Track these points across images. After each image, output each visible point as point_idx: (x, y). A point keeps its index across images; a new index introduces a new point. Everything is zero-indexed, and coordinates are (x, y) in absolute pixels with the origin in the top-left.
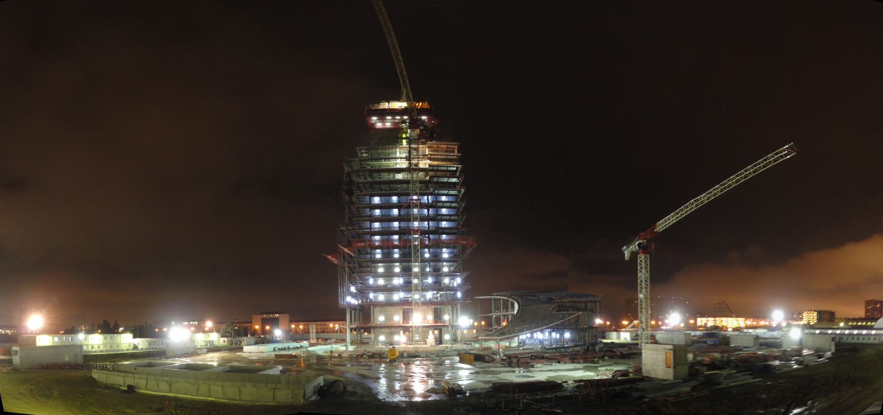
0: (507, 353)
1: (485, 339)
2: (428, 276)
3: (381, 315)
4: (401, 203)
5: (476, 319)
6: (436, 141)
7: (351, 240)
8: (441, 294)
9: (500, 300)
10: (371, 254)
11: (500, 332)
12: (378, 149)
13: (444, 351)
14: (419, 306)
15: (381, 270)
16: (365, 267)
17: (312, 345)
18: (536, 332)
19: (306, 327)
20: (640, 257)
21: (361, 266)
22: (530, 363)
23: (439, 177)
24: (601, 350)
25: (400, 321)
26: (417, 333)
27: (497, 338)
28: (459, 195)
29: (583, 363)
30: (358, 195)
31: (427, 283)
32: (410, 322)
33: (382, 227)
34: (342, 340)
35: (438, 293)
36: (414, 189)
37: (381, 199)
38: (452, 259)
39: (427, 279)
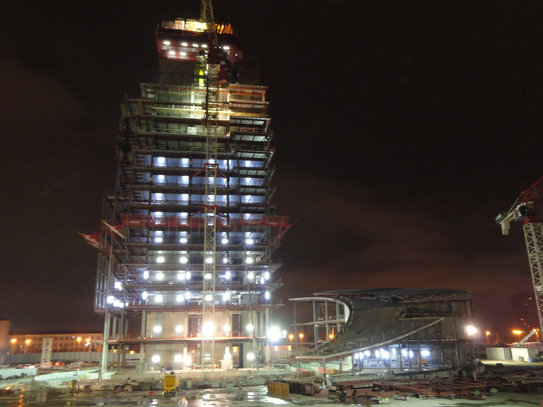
0: (337, 380)
1: (305, 359)
2: (226, 270)
3: (157, 324)
4: (193, 168)
5: (291, 330)
6: (240, 83)
7: (122, 215)
8: (242, 295)
9: (323, 302)
10: (148, 236)
11: (326, 348)
12: (168, 90)
13: (246, 378)
14: (211, 311)
15: (161, 260)
16: (139, 255)
17: (42, 372)
18: (378, 348)
19: (38, 342)
20: (527, 229)
21: (132, 253)
22: (373, 397)
23: (243, 134)
24: (481, 377)
25: (183, 333)
26: (208, 350)
27: (322, 357)
28: (267, 159)
29: (456, 397)
30: (137, 153)
31: (224, 279)
32: (198, 334)
33: (166, 201)
34: (94, 362)
35: (238, 294)
36: (211, 150)
37: (167, 160)
38: (257, 247)
39: (224, 273)
